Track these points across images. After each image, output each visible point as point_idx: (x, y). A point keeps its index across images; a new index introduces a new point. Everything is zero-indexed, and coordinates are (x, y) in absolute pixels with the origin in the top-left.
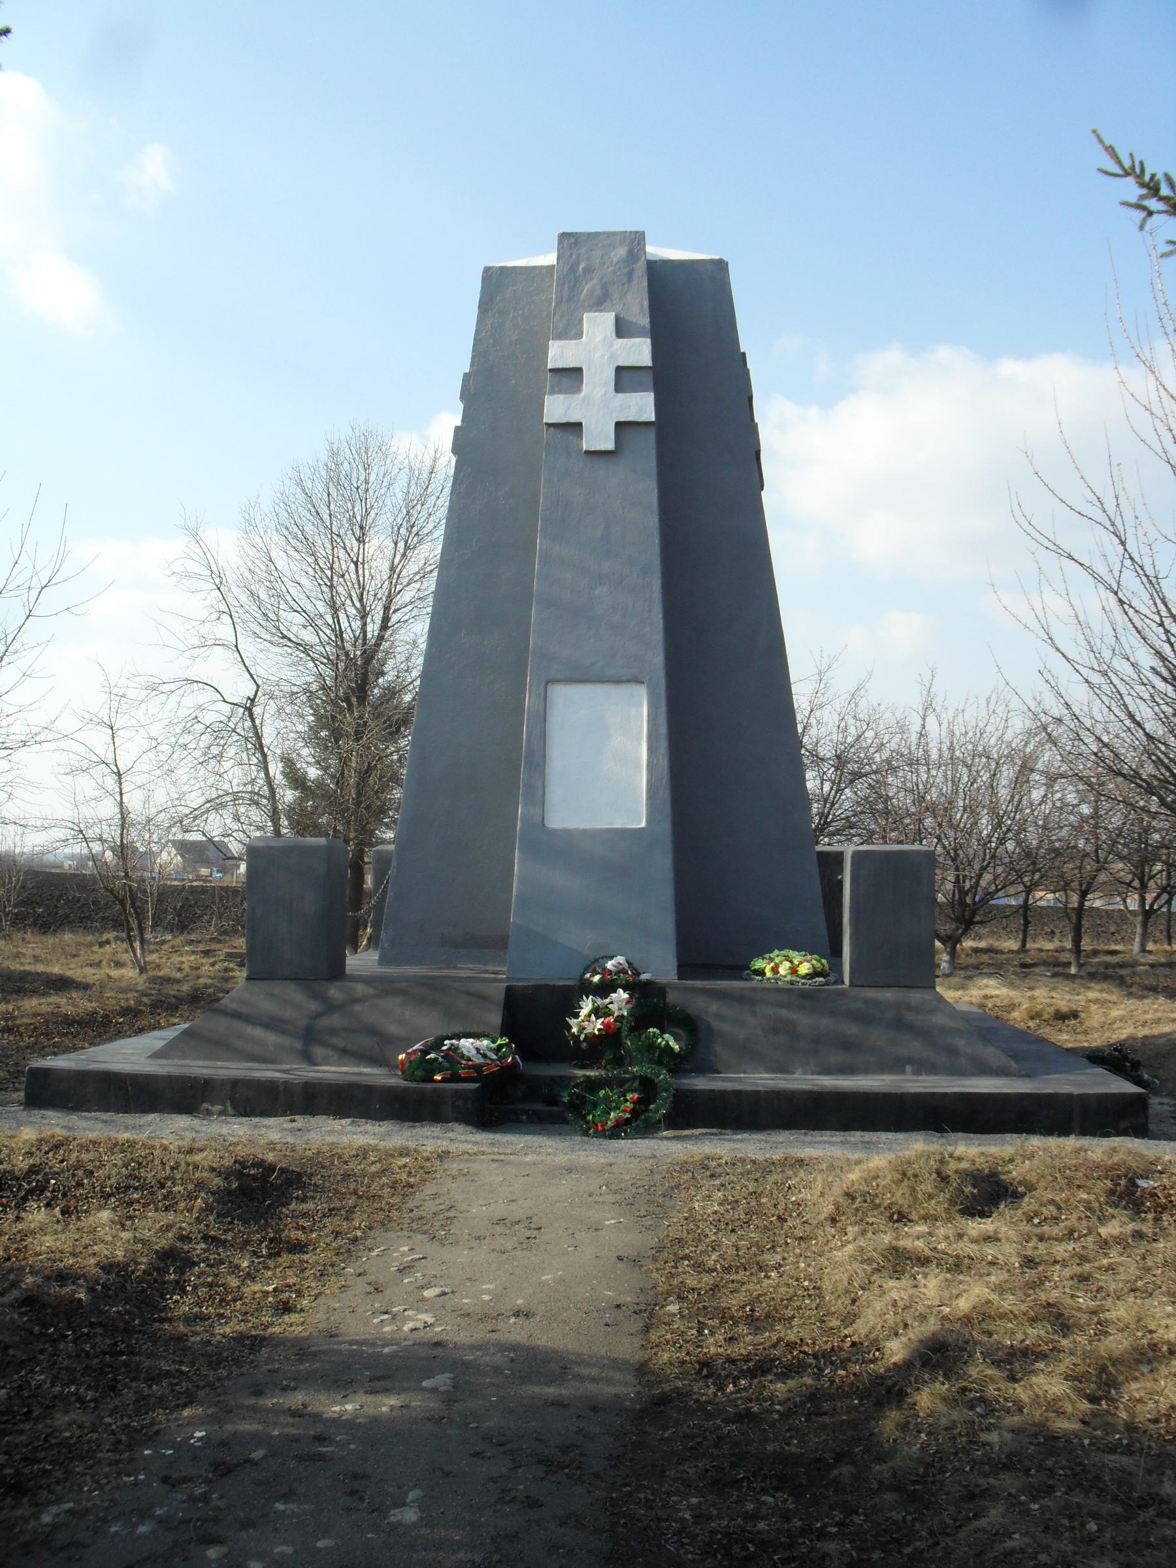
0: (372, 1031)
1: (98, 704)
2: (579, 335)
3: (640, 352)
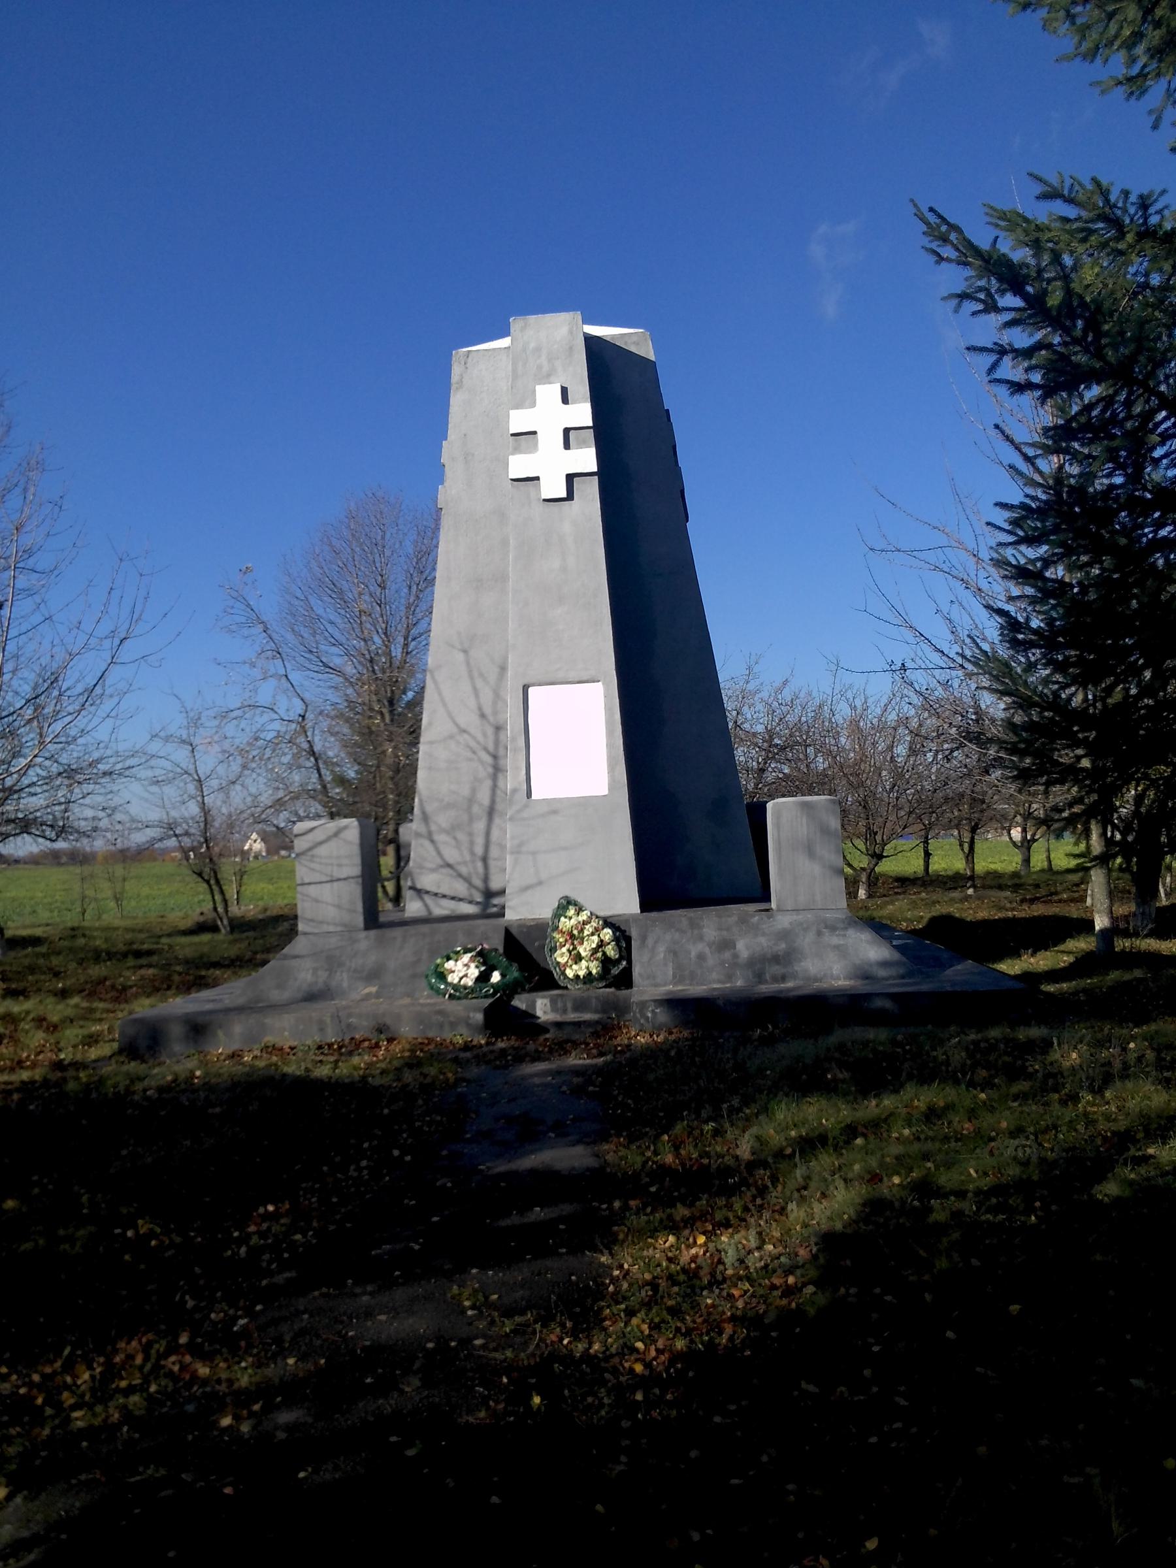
1: (177, 725)
3: (582, 414)
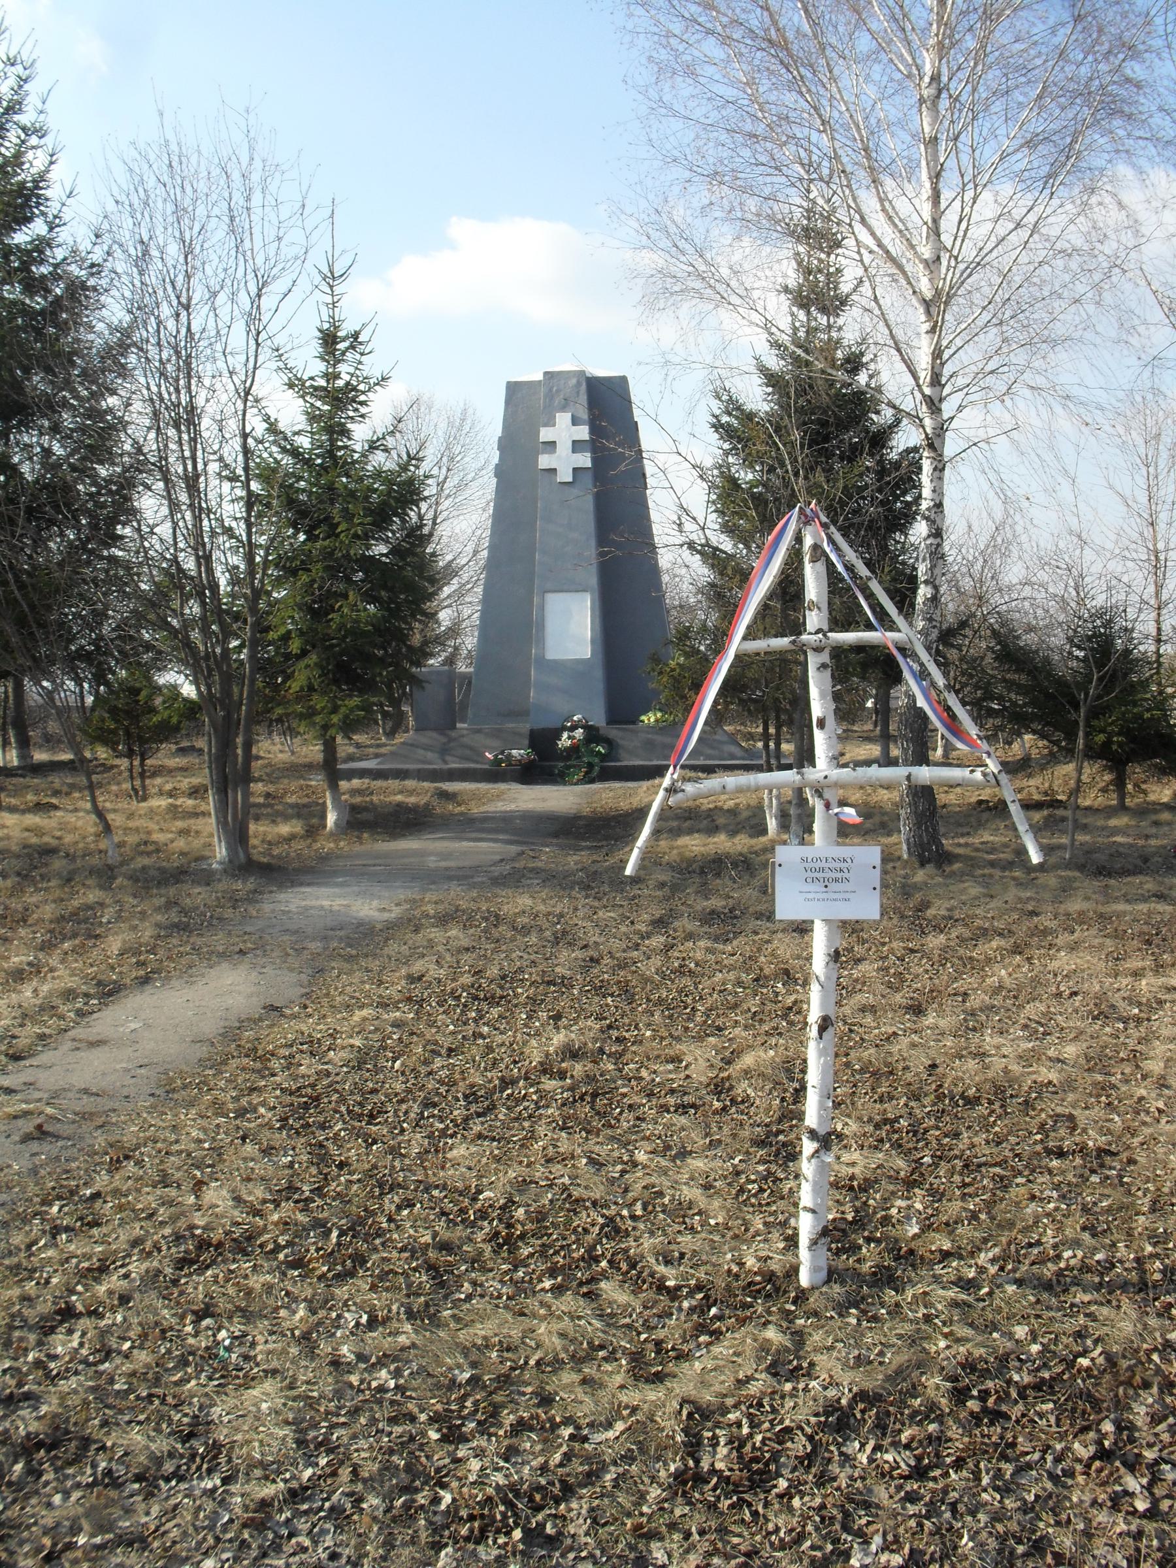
0: (471, 748)
3: (583, 432)
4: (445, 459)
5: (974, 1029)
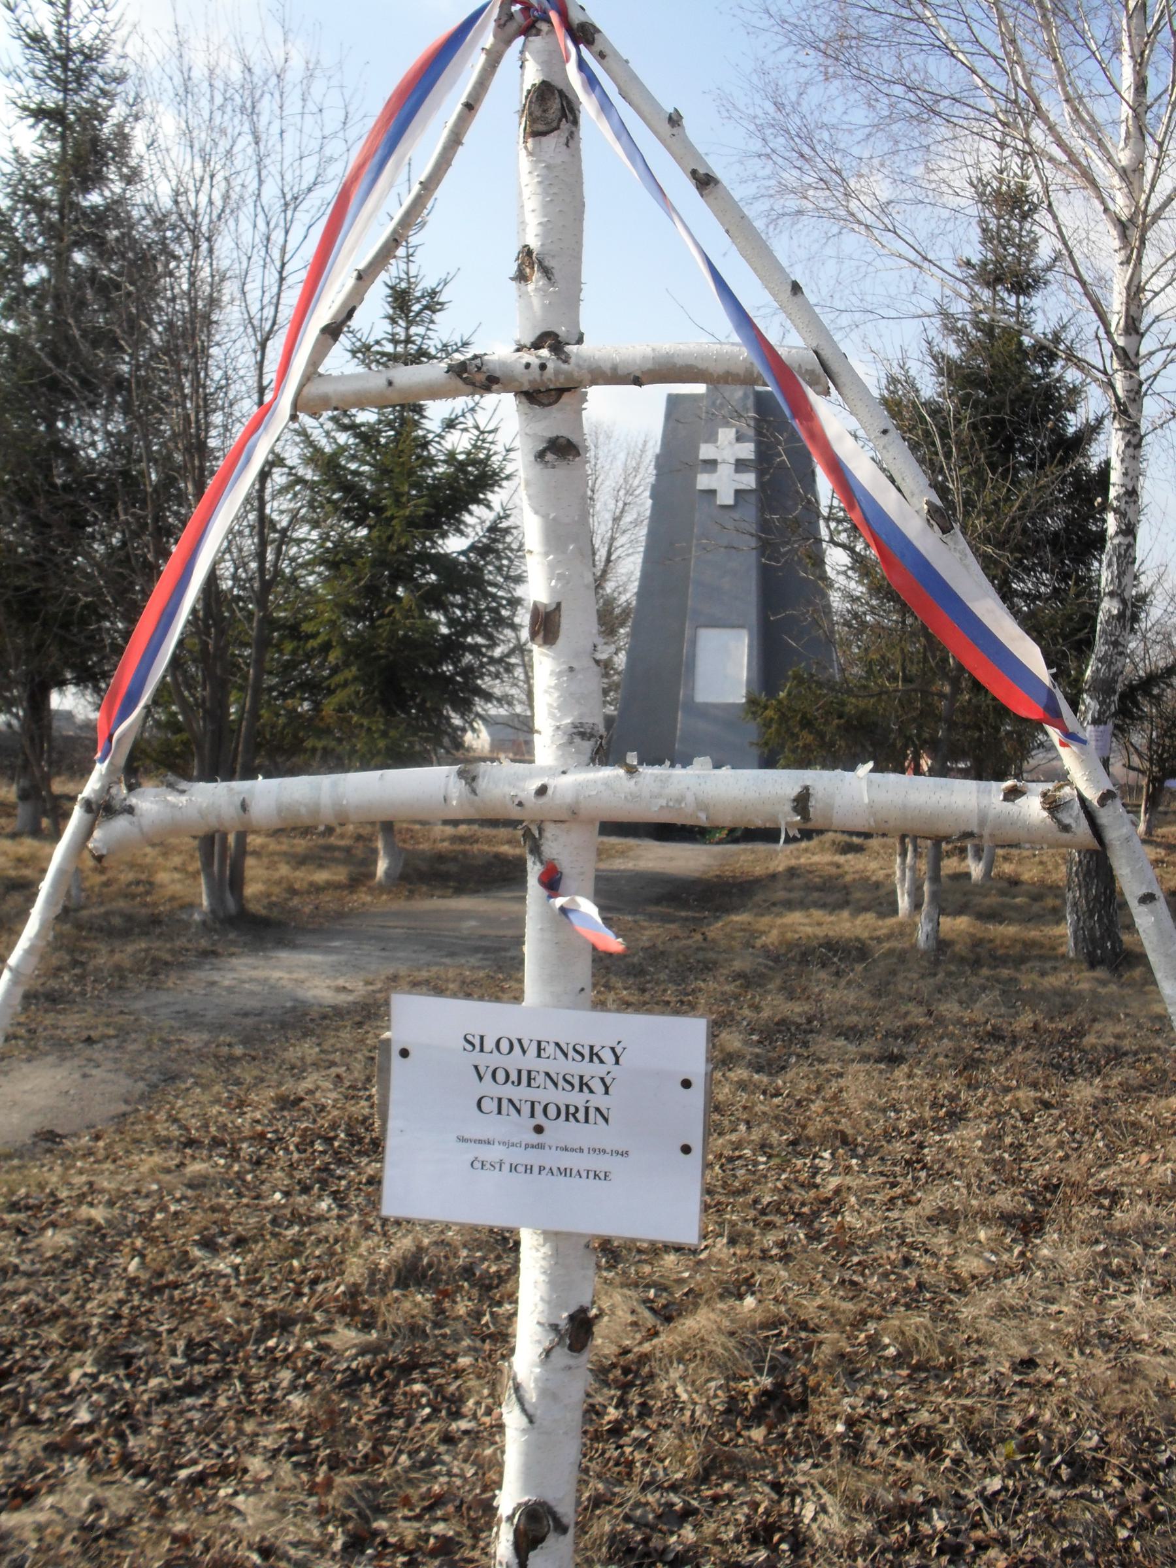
2: (716, 441)
3: (747, 451)
4: (622, 492)
5: (1118, 1274)
